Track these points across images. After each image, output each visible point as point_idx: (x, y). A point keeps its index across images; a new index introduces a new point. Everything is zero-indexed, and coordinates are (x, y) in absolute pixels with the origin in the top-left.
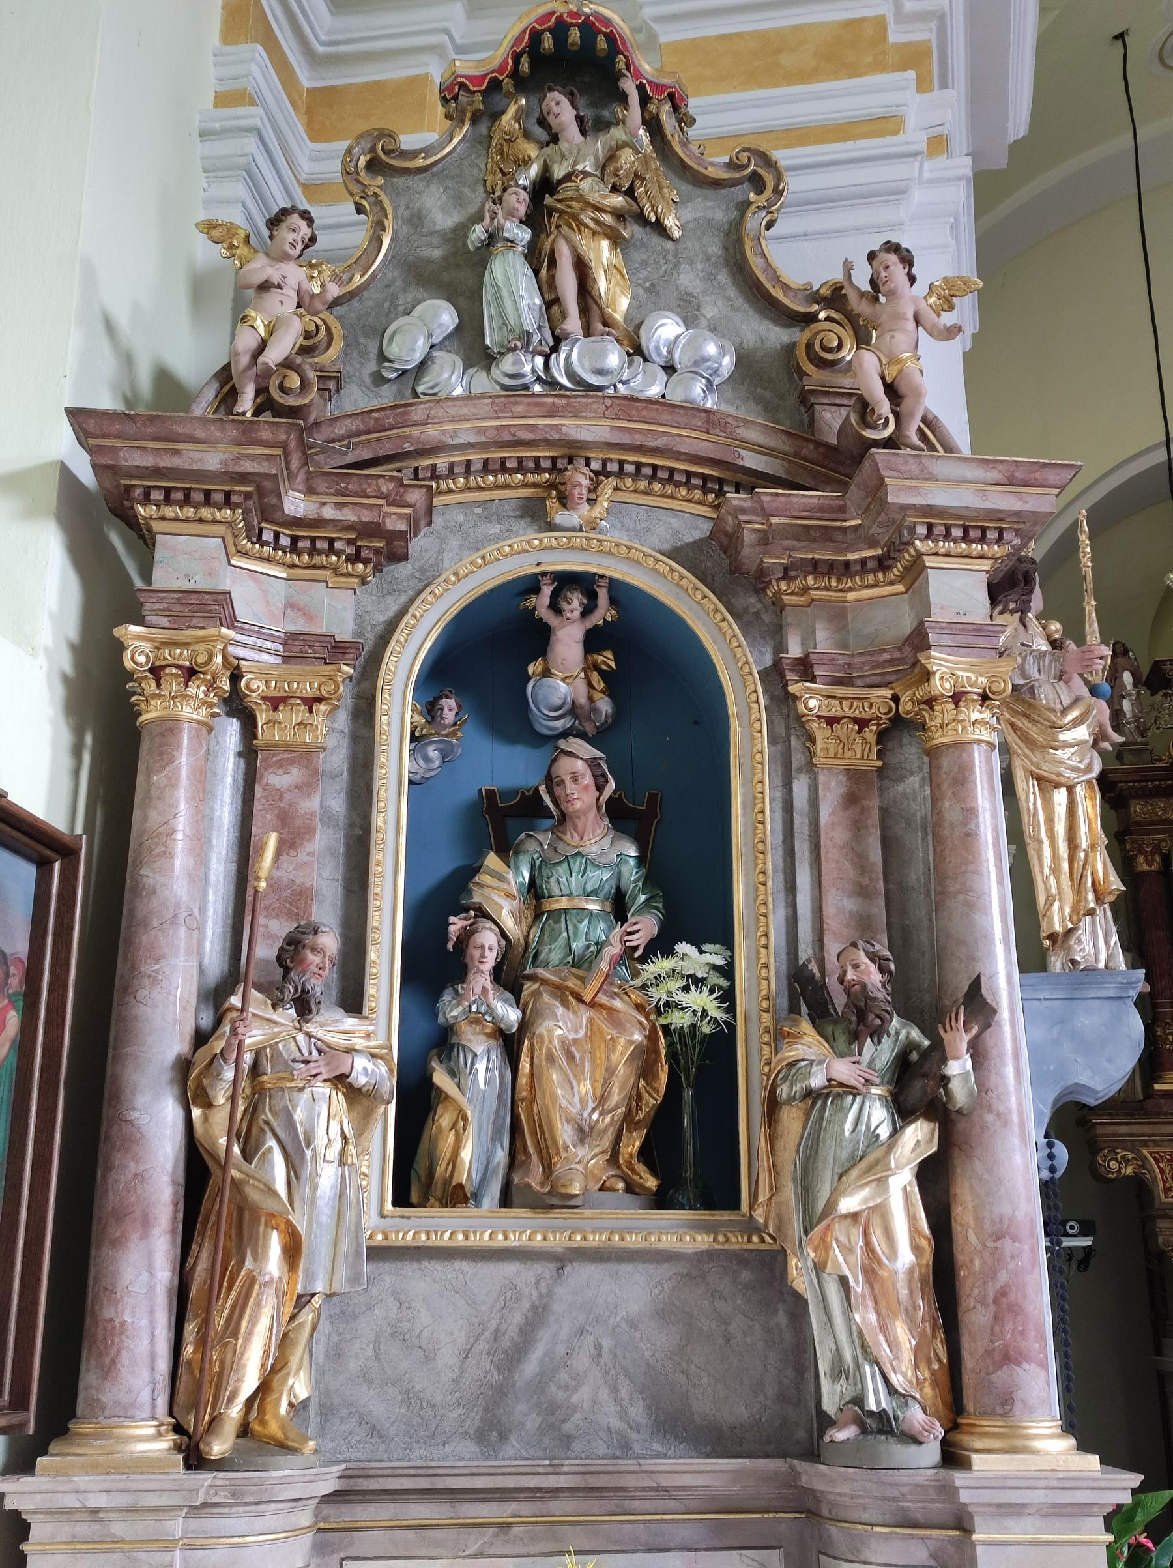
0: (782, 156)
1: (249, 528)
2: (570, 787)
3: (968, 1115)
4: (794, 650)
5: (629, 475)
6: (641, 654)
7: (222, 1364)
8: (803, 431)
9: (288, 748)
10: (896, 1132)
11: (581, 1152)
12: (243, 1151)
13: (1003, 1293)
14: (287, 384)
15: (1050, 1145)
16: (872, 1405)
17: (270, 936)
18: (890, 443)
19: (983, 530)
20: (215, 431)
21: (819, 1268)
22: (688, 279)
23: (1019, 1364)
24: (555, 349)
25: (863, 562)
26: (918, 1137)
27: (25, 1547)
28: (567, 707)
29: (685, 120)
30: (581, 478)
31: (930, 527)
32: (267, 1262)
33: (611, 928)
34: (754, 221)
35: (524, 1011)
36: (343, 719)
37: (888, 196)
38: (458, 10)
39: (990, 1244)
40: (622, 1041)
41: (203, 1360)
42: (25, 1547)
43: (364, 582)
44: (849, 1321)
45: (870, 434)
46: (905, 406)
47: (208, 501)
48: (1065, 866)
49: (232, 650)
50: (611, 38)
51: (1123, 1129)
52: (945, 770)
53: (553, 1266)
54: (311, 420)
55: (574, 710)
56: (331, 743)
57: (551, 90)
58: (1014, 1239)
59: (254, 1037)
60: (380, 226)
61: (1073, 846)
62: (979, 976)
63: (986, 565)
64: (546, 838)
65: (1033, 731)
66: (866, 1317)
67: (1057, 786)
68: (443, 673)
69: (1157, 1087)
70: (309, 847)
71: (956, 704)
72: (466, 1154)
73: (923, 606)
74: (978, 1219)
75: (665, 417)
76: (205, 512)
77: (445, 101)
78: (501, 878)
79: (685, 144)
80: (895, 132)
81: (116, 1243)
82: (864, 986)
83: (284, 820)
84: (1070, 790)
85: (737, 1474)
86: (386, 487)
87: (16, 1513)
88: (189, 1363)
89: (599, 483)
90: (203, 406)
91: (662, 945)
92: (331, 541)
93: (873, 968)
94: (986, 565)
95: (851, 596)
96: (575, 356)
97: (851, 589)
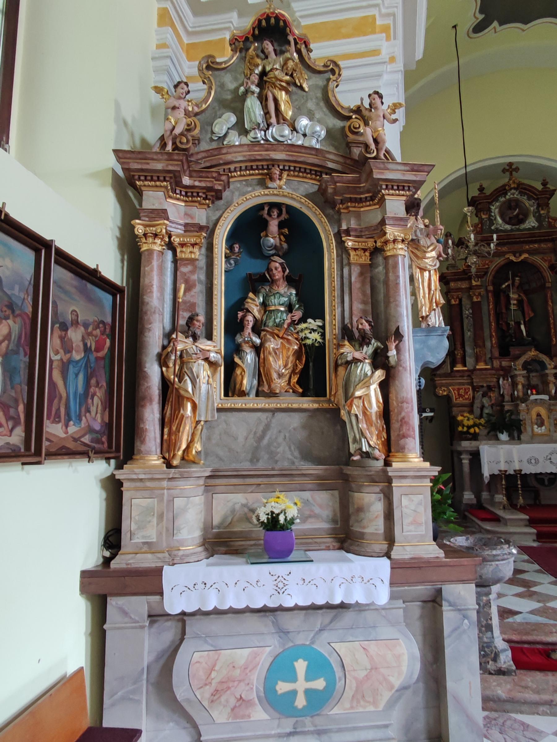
0: (341, 63)
1: (172, 188)
2: (274, 271)
3: (395, 368)
4: (344, 227)
5: (292, 170)
6: (297, 228)
7: (175, 440)
8: (347, 157)
9: (187, 259)
10: (373, 373)
11: (279, 381)
12: (179, 380)
13: (403, 418)
14: (182, 141)
15: (419, 379)
16: (364, 450)
17: (183, 317)
18: (375, 158)
19: (404, 186)
20: (160, 157)
21: (349, 413)
22: (311, 105)
23: (407, 438)
24: (268, 129)
25: (366, 198)
26: (379, 374)
27: (122, 489)
28: (273, 247)
29: (309, 50)
30: (276, 171)
31: (387, 186)
32: (187, 411)
33: (288, 315)
34: (332, 85)
35: (261, 340)
36: (203, 250)
37: (375, 69)
38: (235, 15)
39: (400, 405)
40: (291, 349)
41: (170, 439)
42: (122, 489)
43: (209, 207)
44: (358, 427)
45: (368, 156)
46: (380, 145)
47: (158, 180)
48: (427, 295)
49: (168, 228)
50: (285, 21)
51: (444, 381)
52: (390, 263)
53: (271, 414)
54: (190, 153)
55: (275, 248)
56: (200, 258)
57: (265, 40)
58: (407, 403)
59: (180, 347)
60: (210, 88)
61: (430, 289)
62: (398, 327)
63: (404, 198)
64: (267, 288)
65: (418, 253)
66: (363, 425)
67: (425, 270)
68: (234, 237)
69: (455, 369)
70: (194, 290)
71: (394, 243)
72: (245, 382)
73: (384, 211)
74: (397, 398)
75: (303, 151)
76: (158, 183)
77: (231, 45)
78: (254, 300)
79: (310, 58)
80: (379, 55)
81: (143, 406)
82: (364, 330)
83: (187, 282)
84: (430, 272)
85: (326, 469)
86: (215, 175)
87: (119, 480)
88: (166, 440)
89: (282, 173)
90: (156, 149)
91: (303, 320)
92: (198, 193)
93: (367, 324)
94: (404, 198)
95: (362, 209)
96: (273, 130)
97: (362, 207)
